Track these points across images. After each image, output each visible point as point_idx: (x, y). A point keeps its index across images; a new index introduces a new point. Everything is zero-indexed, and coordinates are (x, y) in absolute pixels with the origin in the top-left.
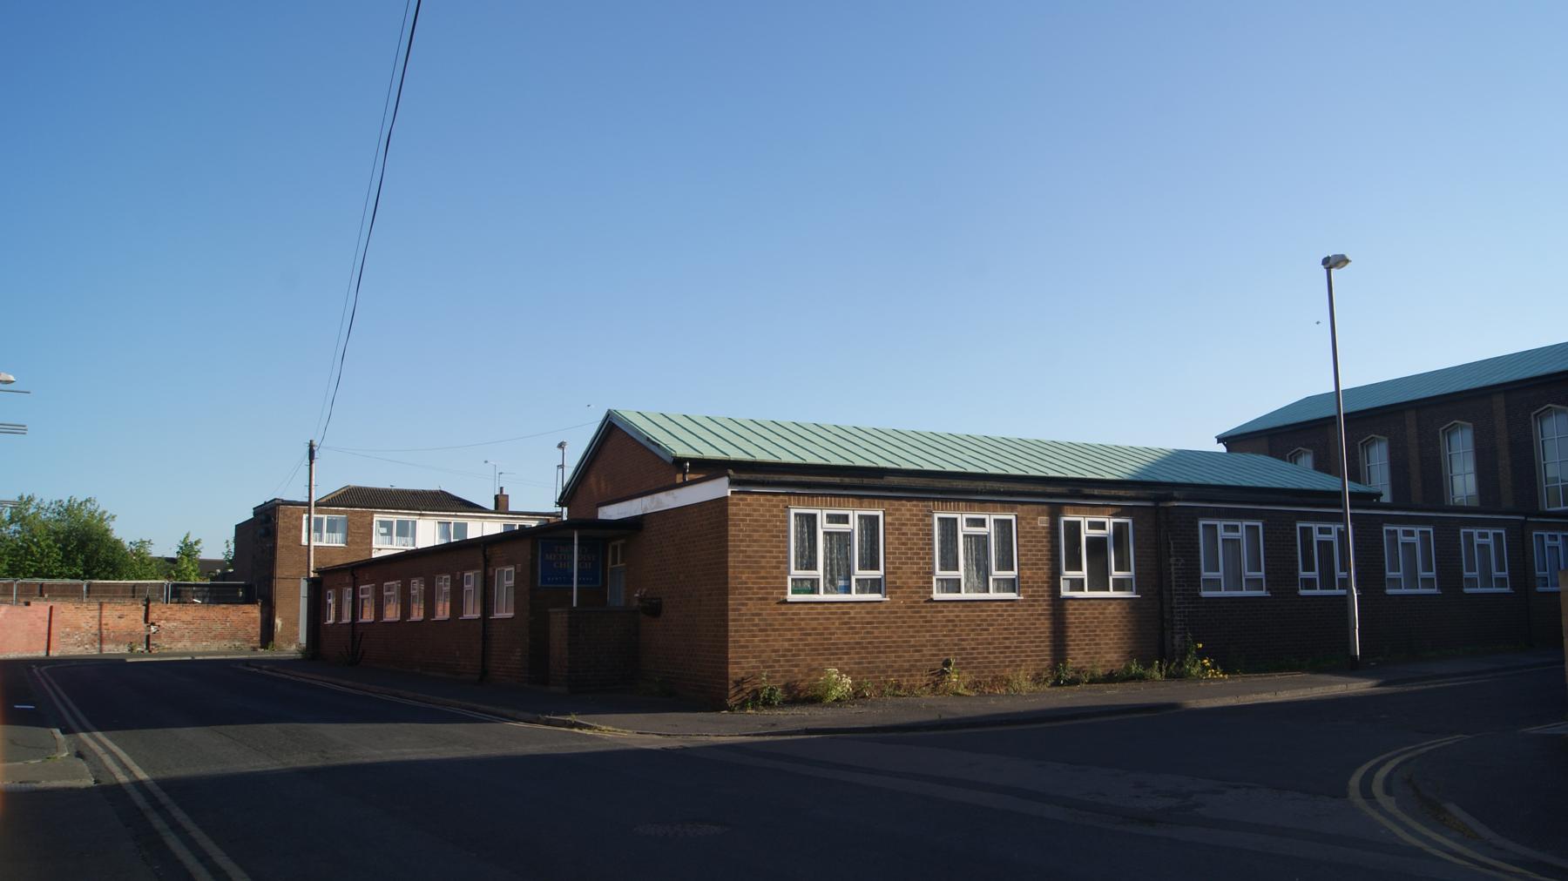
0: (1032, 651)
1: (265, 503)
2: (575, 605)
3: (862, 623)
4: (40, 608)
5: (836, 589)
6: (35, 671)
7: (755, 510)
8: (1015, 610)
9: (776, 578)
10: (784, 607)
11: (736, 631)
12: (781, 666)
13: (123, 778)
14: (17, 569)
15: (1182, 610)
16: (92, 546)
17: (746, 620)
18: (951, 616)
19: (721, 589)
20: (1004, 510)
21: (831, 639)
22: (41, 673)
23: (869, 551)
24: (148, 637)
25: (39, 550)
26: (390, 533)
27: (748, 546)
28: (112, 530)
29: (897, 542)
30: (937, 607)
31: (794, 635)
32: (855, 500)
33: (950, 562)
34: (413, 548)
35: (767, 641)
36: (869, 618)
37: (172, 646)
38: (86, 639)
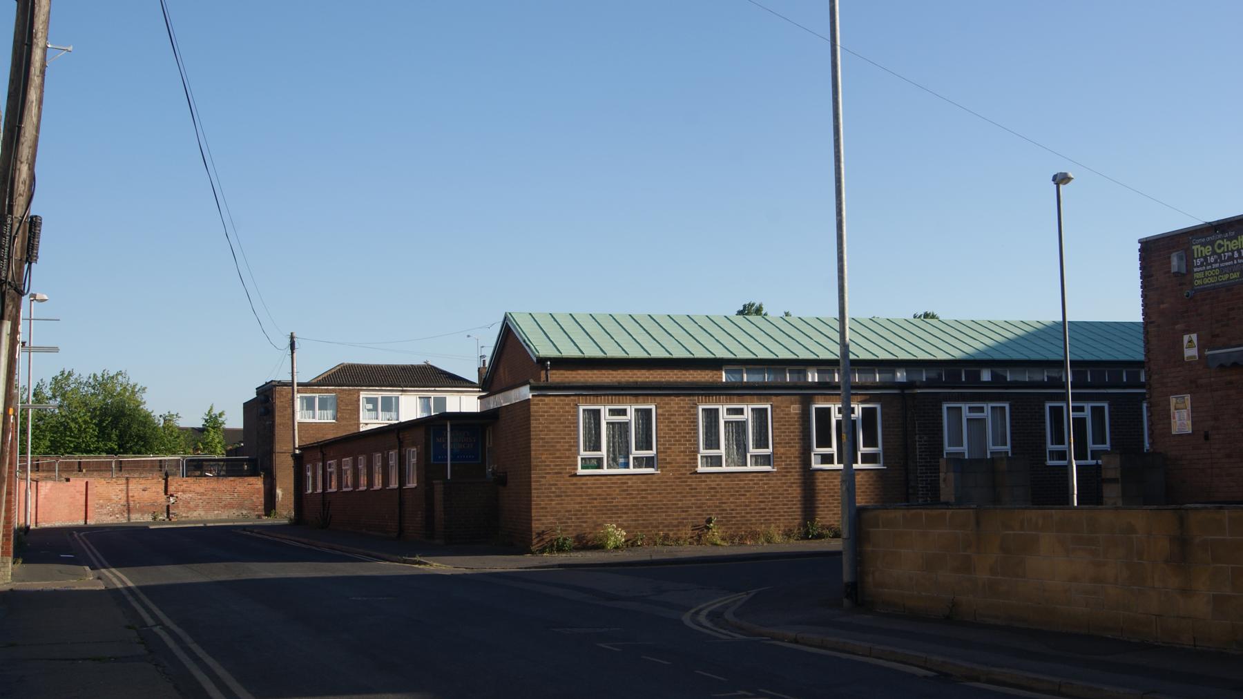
0: (785, 512)
1: (266, 383)
2: (449, 478)
3: (638, 490)
4: (78, 483)
5: (618, 465)
6: (76, 536)
7: (551, 408)
8: (770, 480)
9: (569, 457)
10: (575, 480)
11: (537, 497)
12: (573, 522)
13: (120, 586)
14: (59, 445)
15: (924, 478)
16: (125, 421)
17: (545, 489)
18: (713, 485)
19: (529, 468)
20: (760, 401)
21: (613, 502)
22: (80, 537)
23: (644, 436)
24: (168, 506)
25: (77, 426)
26: (375, 409)
27: (546, 435)
28: (145, 402)
29: (667, 428)
30: (701, 478)
31: (583, 499)
32: (631, 397)
33: (712, 442)
34: (397, 422)
35: (562, 504)
36: (643, 486)
37: (189, 515)
38: (116, 509)
